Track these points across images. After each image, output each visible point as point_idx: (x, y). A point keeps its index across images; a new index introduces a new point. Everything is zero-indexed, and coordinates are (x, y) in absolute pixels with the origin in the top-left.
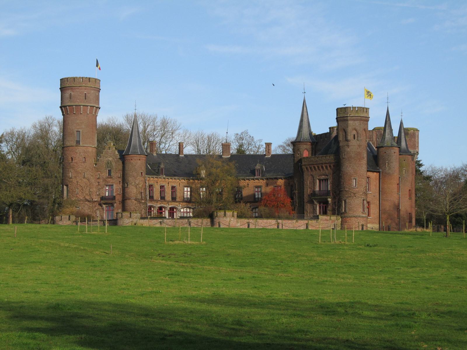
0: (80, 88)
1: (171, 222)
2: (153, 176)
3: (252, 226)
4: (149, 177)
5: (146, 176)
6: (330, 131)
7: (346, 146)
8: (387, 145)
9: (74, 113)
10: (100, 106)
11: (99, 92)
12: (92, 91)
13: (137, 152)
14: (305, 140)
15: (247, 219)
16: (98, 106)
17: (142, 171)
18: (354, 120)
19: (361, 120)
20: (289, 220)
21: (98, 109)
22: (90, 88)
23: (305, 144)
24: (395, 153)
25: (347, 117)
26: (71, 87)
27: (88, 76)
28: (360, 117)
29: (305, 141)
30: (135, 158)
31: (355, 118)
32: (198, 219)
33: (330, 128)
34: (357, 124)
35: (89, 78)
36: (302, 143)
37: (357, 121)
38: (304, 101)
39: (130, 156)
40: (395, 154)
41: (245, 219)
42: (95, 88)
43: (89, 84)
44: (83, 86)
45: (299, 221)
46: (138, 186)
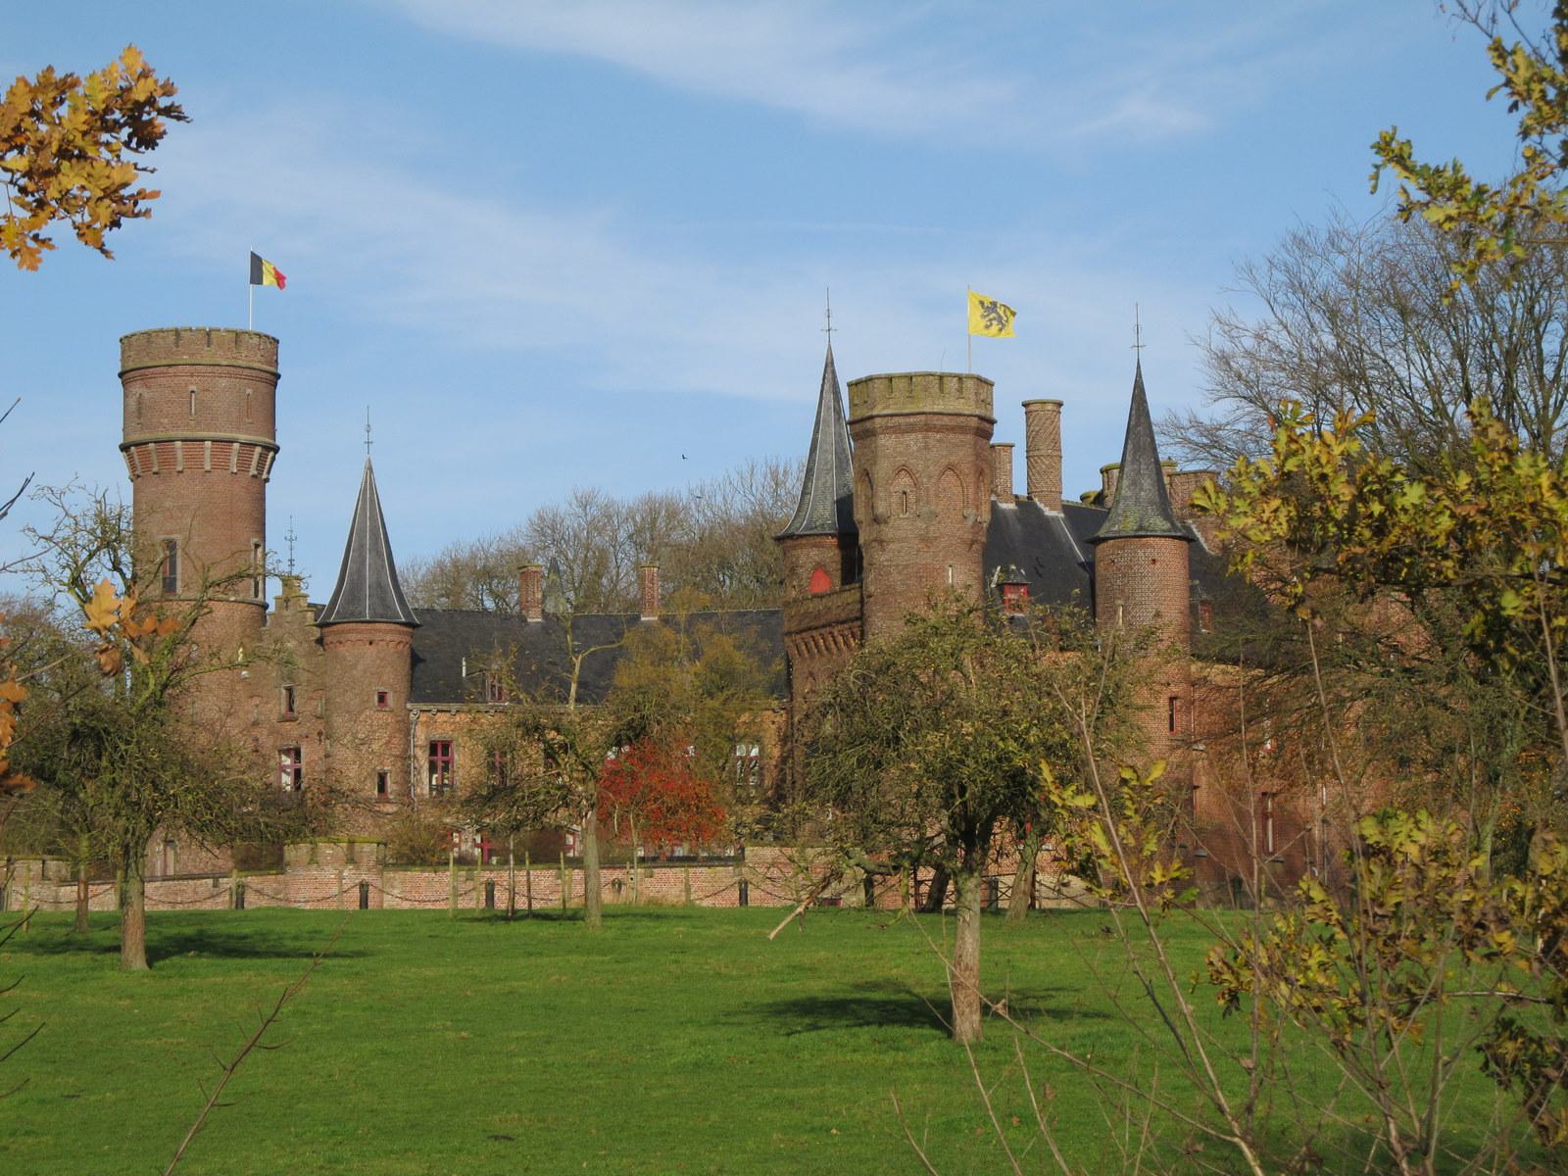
0: (171, 370)
1: (161, 891)
2: (444, 706)
3: (252, 901)
4: (425, 708)
5: (409, 706)
6: (1107, 483)
7: (874, 544)
8: (1119, 531)
9: (155, 469)
10: (277, 443)
11: (275, 385)
12: (224, 382)
13: (360, 613)
14: (812, 529)
15: (429, 869)
16: (271, 441)
17: (382, 689)
18: (898, 430)
19: (928, 428)
20: (615, 868)
21: (271, 454)
22: (210, 369)
23: (815, 546)
24: (1154, 561)
25: (872, 417)
26: (143, 371)
27: (207, 324)
28: (923, 417)
29: (816, 531)
30: (353, 636)
31: (901, 420)
32: (246, 876)
33: (1105, 471)
34: (915, 448)
35: (177, 332)
36: (804, 541)
37: (913, 436)
38: (1139, 374)
39: (335, 628)
40: (1158, 565)
41: (423, 871)
42: (232, 369)
43: (207, 355)
44: (181, 362)
45: (656, 870)
46: (364, 748)
